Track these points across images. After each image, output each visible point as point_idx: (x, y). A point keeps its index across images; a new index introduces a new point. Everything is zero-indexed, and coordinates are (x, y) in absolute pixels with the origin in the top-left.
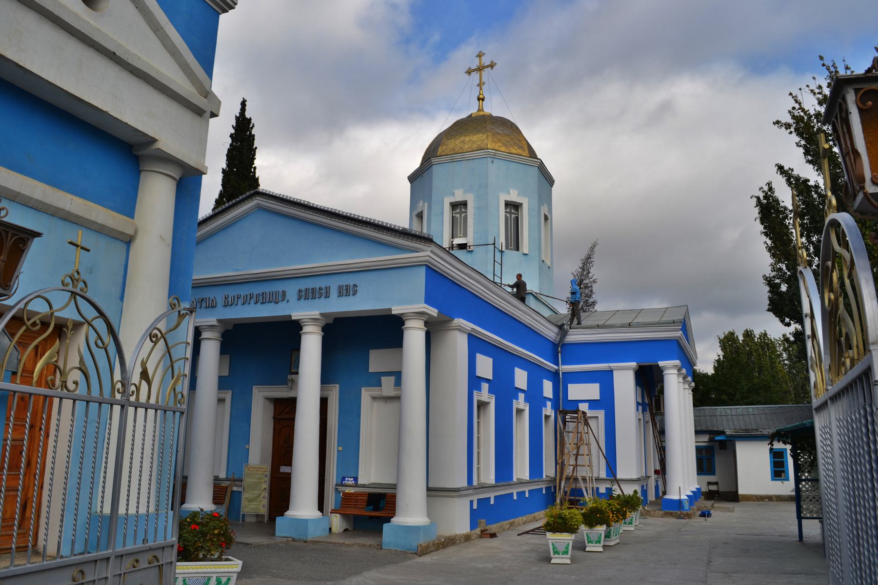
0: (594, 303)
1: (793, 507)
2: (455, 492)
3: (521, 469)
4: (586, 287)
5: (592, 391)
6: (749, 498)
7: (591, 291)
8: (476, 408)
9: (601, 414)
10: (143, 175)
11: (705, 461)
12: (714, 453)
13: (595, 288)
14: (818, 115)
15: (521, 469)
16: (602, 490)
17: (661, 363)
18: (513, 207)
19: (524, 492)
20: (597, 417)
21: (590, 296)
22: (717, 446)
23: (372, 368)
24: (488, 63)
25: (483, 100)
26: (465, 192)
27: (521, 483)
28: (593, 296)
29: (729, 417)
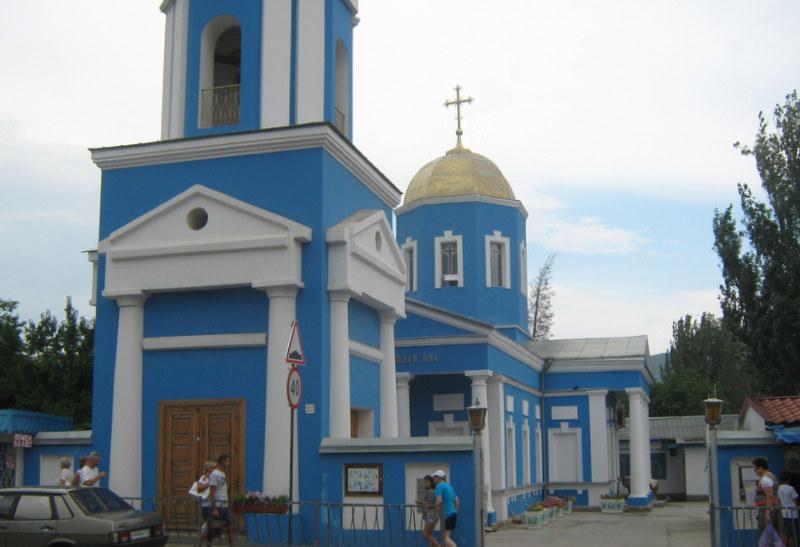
0: (551, 315)
1: (286, 123)
2: (503, 492)
3: (527, 479)
4: (544, 297)
5: (571, 412)
6: (146, 528)
7: (549, 302)
8: (508, 432)
9: (579, 431)
10: (332, 304)
11: (659, 466)
12: (667, 456)
13: (553, 300)
14: (774, 140)
15: (527, 479)
16: (580, 492)
17: (627, 390)
18: (500, 246)
19: (522, 495)
20: (575, 434)
21: (547, 308)
22: (668, 453)
23: (437, 408)
24: (466, 98)
25: (461, 133)
26: (454, 234)
27: (529, 487)
28: (551, 308)
29: (680, 428)
